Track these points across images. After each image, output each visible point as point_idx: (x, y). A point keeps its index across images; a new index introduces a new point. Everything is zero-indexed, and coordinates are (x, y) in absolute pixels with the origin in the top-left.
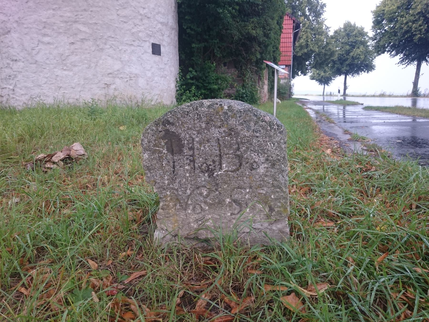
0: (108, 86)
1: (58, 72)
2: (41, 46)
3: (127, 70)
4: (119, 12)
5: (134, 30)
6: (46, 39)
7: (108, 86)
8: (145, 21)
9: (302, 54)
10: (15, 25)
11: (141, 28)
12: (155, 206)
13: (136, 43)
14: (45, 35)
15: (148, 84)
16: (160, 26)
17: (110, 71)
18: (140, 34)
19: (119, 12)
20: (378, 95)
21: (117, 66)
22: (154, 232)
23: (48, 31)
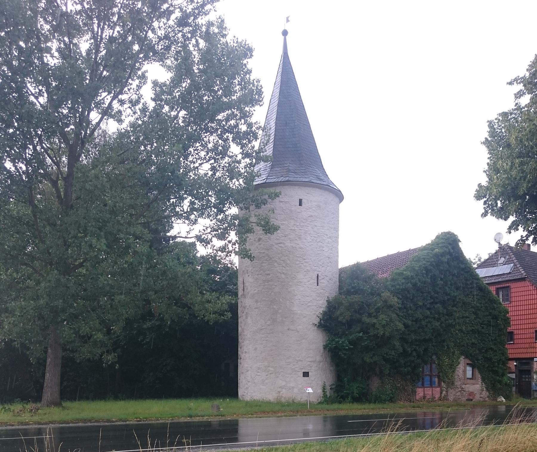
0: (279, 392)
3: (288, 385)
6: (258, 374)
7: (279, 392)
8: (300, 363)
11: (297, 366)
12: (275, 264)
14: (258, 372)
16: (309, 363)
20: (485, 257)
21: (284, 383)
23: (259, 371)
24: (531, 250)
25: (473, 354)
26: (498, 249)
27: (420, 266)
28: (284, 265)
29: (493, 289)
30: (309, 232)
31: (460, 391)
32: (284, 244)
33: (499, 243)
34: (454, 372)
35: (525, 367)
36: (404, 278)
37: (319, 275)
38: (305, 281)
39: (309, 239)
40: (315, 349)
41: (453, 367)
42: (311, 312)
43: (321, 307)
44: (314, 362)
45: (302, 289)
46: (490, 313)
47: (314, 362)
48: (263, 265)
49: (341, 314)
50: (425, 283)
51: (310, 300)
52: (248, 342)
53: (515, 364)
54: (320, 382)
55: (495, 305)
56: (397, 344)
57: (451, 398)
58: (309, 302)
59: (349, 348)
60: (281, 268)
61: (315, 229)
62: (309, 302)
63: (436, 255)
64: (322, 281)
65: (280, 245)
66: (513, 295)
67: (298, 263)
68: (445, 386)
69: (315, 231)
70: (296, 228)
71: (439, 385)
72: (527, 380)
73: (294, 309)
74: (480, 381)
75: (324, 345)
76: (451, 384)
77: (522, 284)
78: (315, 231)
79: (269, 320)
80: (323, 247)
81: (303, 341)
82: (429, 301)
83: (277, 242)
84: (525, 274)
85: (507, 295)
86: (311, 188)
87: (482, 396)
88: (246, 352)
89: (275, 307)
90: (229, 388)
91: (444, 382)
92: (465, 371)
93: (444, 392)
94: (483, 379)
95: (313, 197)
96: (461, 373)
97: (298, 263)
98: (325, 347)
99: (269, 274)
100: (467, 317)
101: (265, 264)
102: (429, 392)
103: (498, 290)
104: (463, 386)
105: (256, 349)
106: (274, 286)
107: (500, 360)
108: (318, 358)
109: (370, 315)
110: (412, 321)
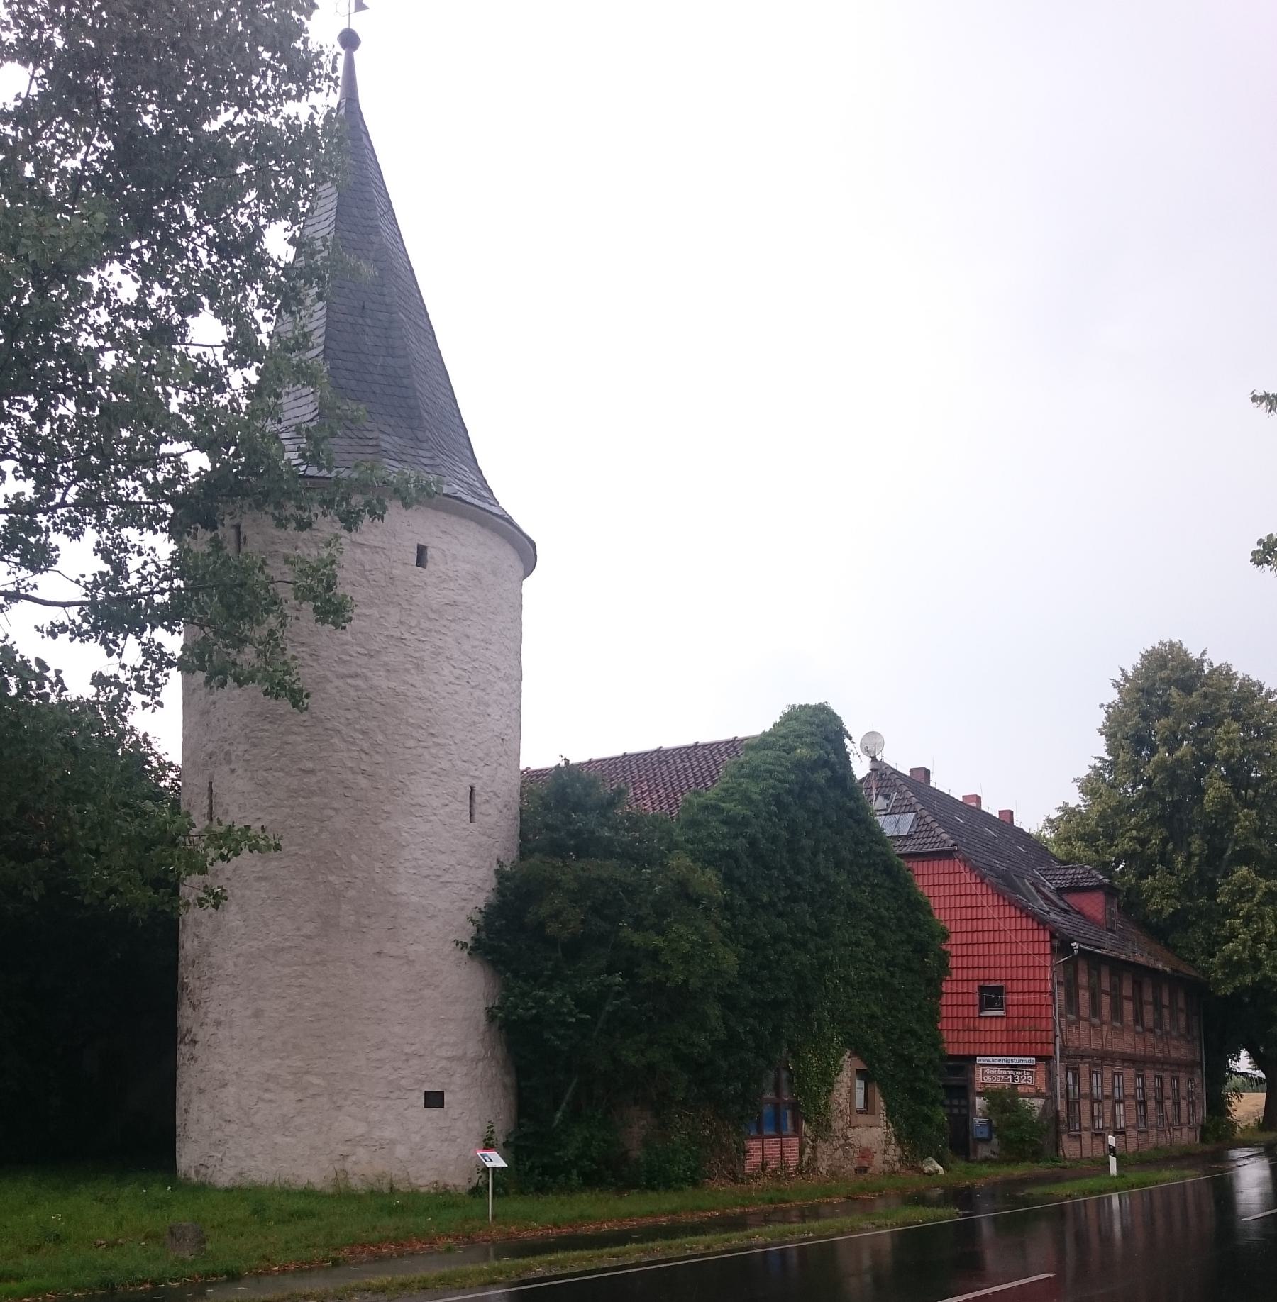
1: (279, 1139)
2: (261, 1105)
3: (377, 1134)
4: (370, 1055)
5: (391, 1078)
6: (267, 1096)
7: (344, 1157)
8: (414, 1062)
9: (1235, 988)
10: (234, 1077)
11: (404, 1073)
12: (335, 740)
13: (393, 1096)
14: (267, 1090)
15: (412, 1154)
16: (443, 1063)
17: (348, 1137)
18: (403, 1082)
19: (370, 1055)
21: (361, 1129)
22: (339, 104)
23: (271, 1085)
24: (932, 785)
25: (871, 1046)
27: (763, 791)
28: (365, 746)
31: (842, 1146)
32: (366, 679)
33: (874, 759)
34: (829, 1091)
35: (955, 1080)
36: (724, 822)
37: (477, 788)
39: (446, 672)
40: (465, 1019)
41: (827, 1078)
42: (453, 902)
43: (480, 889)
44: (459, 1059)
45: (424, 828)
46: (910, 936)
47: (459, 1059)
48: (291, 738)
49: (556, 915)
50: (774, 839)
51: (446, 866)
52: (227, 989)
54: (477, 1124)
55: (921, 916)
56: (714, 1011)
57: (823, 1165)
59: (579, 1020)
60: (355, 755)
61: (466, 646)
63: (799, 765)
64: (484, 808)
65: (349, 681)
67: (411, 743)
68: (809, 1133)
69: (464, 653)
70: (406, 635)
71: (797, 1131)
73: (401, 889)
74: (883, 1117)
75: (488, 1010)
76: (823, 1128)
77: (943, 866)
79: (312, 920)
80: (487, 705)
81: (427, 992)
82: (782, 894)
83: (342, 670)
84: (952, 842)
86: (454, 518)
87: (888, 1158)
88: (218, 1023)
89: (332, 878)
90: (144, 1140)
91: (807, 1121)
92: (851, 1092)
93: (808, 1150)
94: (891, 1113)
95: (459, 548)
96: (845, 1095)
97: (411, 743)
98: (491, 1015)
99: (311, 772)
100: (857, 944)
101: (299, 739)
102: (773, 1148)
104: (850, 1133)
105: (258, 1014)
106: (331, 813)
107: (930, 1062)
108: (473, 1048)
109: (638, 924)
110: (746, 947)
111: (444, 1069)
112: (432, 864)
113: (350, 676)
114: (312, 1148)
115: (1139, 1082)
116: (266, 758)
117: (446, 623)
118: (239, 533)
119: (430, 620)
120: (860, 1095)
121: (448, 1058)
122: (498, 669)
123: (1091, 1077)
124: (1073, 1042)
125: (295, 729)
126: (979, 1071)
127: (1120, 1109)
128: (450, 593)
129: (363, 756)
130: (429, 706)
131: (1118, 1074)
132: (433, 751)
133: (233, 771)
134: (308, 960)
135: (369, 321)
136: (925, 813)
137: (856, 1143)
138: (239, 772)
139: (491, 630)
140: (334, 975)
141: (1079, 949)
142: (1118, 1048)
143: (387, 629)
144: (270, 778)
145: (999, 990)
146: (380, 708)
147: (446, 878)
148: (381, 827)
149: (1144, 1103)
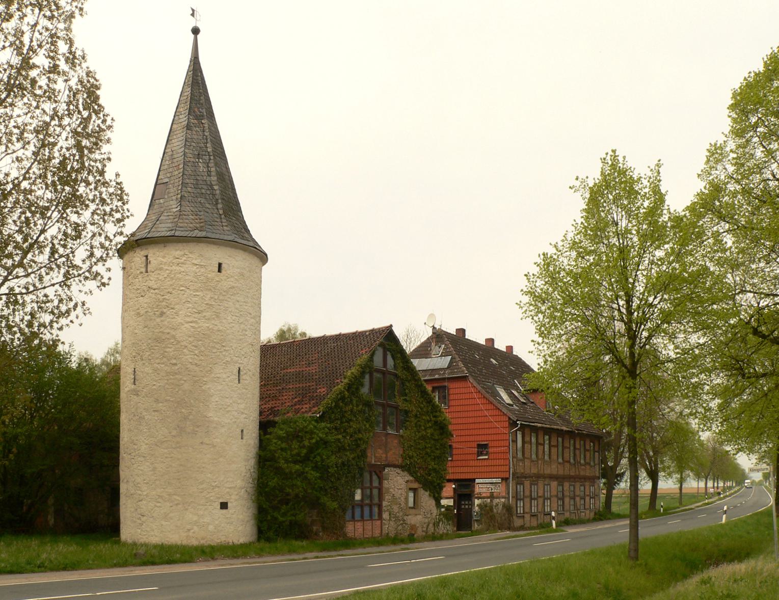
1: (163, 523)
2: (156, 508)
6: (158, 504)
11: (213, 494)
13: (208, 504)
16: (228, 490)
21: (195, 518)
23: (160, 500)
24: (466, 337)
26: (430, 334)
29: (429, 388)
30: (230, 310)
31: (402, 524)
35: (465, 491)
37: (241, 368)
38: (224, 376)
39: (229, 318)
42: (231, 420)
48: (168, 350)
53: (454, 486)
58: (229, 406)
62: (229, 406)
65: (191, 324)
66: (452, 397)
67: (215, 351)
69: (237, 309)
72: (467, 507)
73: (210, 415)
78: (237, 309)
80: (246, 331)
81: (221, 459)
85: (444, 397)
89: (183, 410)
97: (215, 351)
99: (175, 364)
101: (171, 350)
103: (434, 389)
104: (405, 518)
111: (228, 493)
112: (223, 403)
113: (191, 322)
114: (177, 526)
115: (560, 488)
116: (157, 358)
117: (230, 296)
118: (147, 259)
119: (223, 295)
120: (411, 500)
121: (229, 488)
122: (250, 314)
123: (531, 487)
124: (520, 470)
125: (169, 346)
126: (477, 486)
127: (534, 503)
128: (231, 283)
129: (195, 357)
130: (223, 333)
131: (547, 485)
132: (224, 353)
133: (144, 364)
134: (174, 446)
135: (201, 160)
136: (457, 356)
137: (409, 523)
138: (147, 364)
139: (248, 297)
140: (184, 452)
141: (521, 424)
142: (548, 471)
143: (206, 301)
144: (159, 367)
145: (486, 446)
146: (203, 336)
147: (229, 409)
148: (203, 388)
149: (563, 499)
